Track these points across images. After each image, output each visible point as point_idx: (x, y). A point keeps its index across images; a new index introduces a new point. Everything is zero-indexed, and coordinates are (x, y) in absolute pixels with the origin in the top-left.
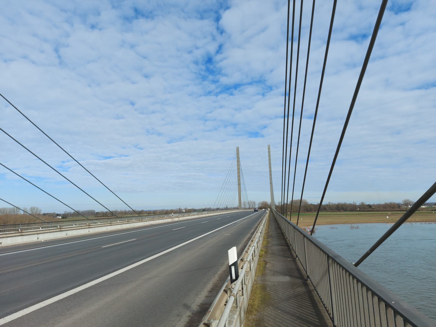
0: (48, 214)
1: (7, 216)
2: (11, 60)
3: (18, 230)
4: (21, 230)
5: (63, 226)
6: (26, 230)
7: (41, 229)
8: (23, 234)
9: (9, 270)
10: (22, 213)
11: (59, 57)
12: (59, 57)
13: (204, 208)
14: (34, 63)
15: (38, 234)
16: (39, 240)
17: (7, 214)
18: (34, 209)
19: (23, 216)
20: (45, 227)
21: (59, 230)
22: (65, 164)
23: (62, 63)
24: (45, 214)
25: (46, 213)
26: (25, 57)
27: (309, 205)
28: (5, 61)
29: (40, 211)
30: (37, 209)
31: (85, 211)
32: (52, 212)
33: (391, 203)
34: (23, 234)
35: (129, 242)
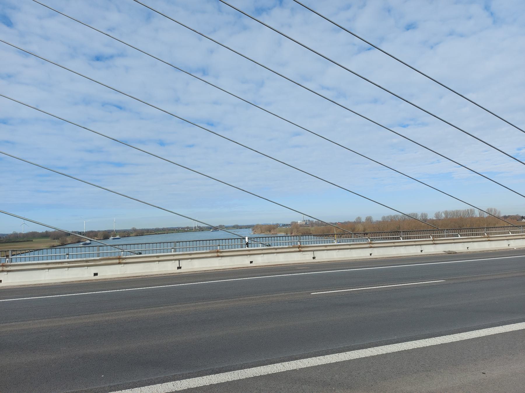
0: (509, 216)
1: (462, 219)
2: (437, 44)
3: (483, 234)
4: (488, 234)
5: (491, 234)
6: (442, 237)
7: (511, 234)
8: (490, 239)
9: (488, 278)
10: (486, 215)
11: (492, 14)
12: (492, 14)
13: (129, 227)
14: (462, 36)
15: (508, 240)
16: (511, 247)
17: (461, 217)
18: (491, 211)
19: (444, 220)
20: (465, 235)
21: (431, 242)
22: (522, 151)
23: (496, 20)
24: (505, 217)
25: (507, 215)
26: (451, 34)
27: (378, 223)
28: (432, 47)
29: (499, 213)
30: (495, 210)
31: (20, 234)
32: (515, 214)
33: (345, 223)
34: (490, 239)
35: (418, 287)
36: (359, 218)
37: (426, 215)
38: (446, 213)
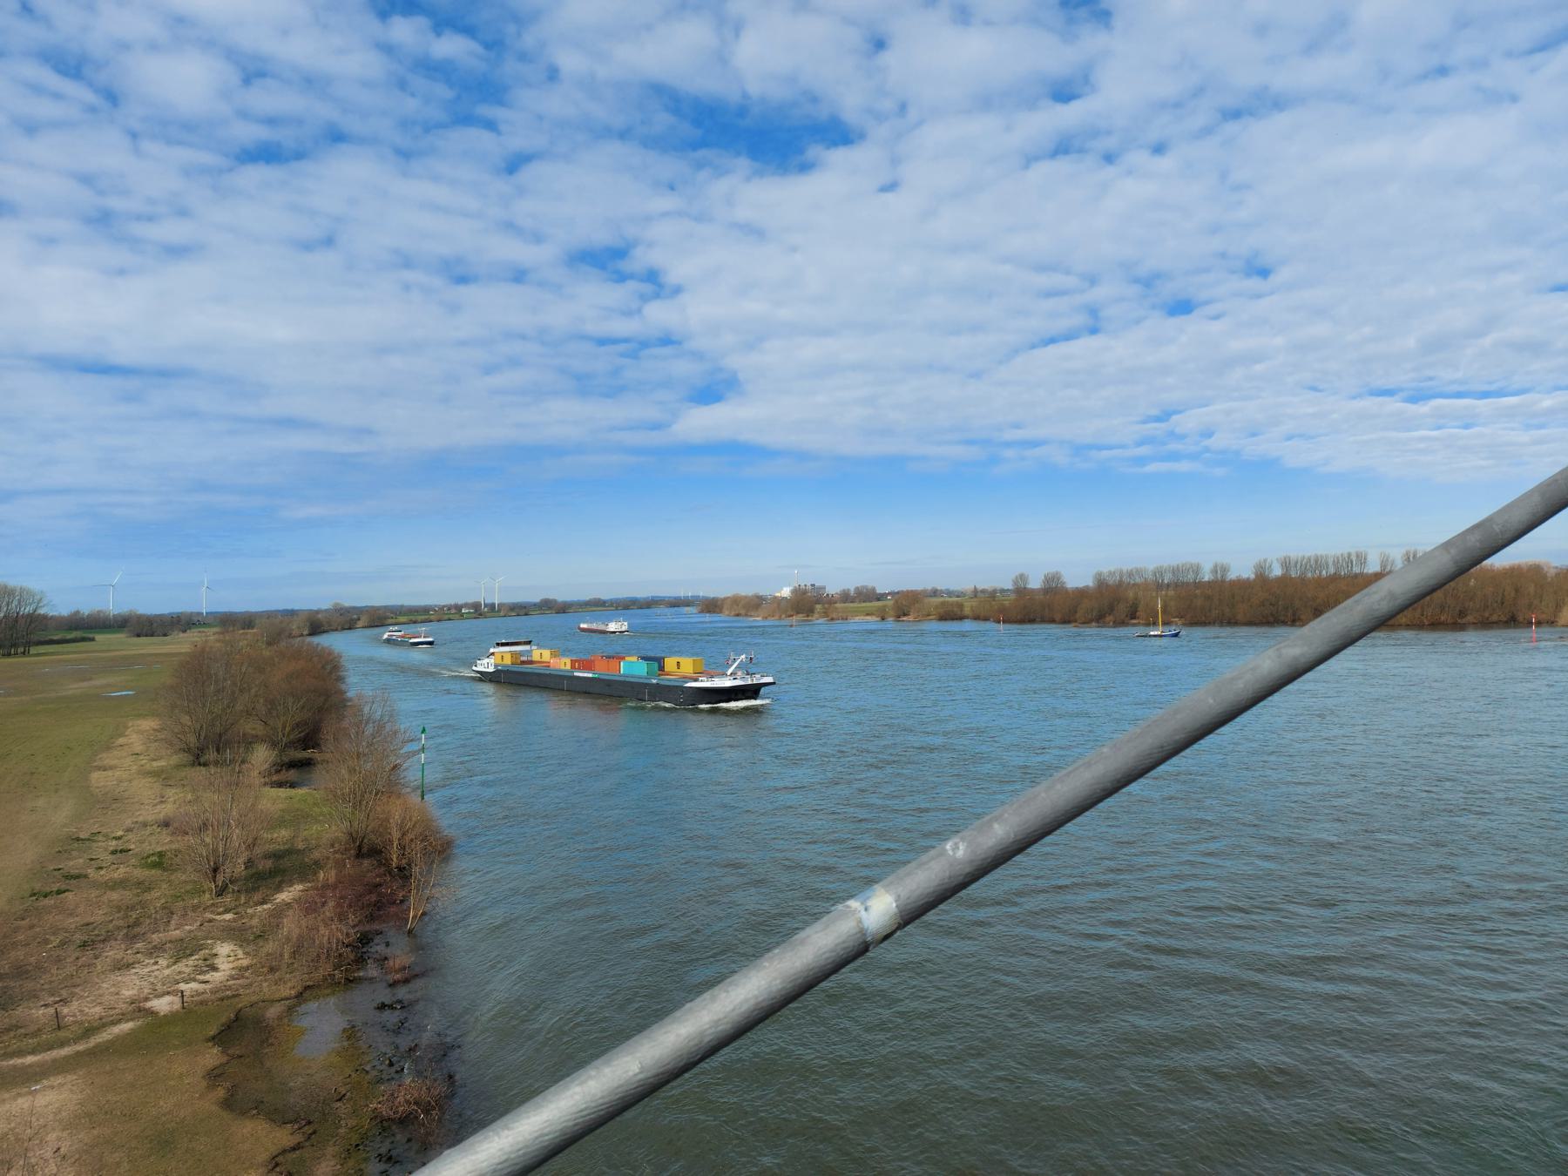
36: (1022, 577)
37: (1225, 569)
38: (1286, 564)
